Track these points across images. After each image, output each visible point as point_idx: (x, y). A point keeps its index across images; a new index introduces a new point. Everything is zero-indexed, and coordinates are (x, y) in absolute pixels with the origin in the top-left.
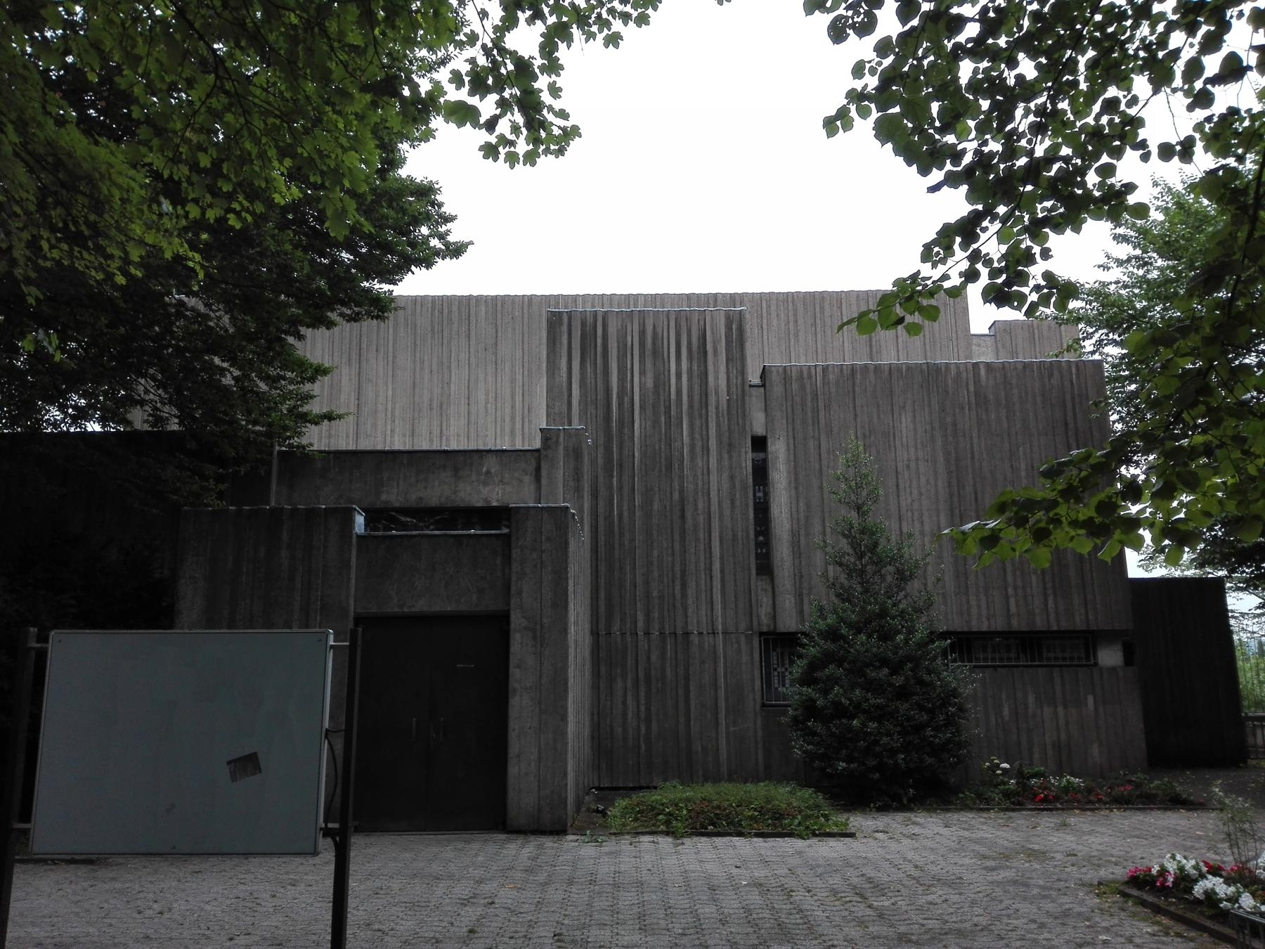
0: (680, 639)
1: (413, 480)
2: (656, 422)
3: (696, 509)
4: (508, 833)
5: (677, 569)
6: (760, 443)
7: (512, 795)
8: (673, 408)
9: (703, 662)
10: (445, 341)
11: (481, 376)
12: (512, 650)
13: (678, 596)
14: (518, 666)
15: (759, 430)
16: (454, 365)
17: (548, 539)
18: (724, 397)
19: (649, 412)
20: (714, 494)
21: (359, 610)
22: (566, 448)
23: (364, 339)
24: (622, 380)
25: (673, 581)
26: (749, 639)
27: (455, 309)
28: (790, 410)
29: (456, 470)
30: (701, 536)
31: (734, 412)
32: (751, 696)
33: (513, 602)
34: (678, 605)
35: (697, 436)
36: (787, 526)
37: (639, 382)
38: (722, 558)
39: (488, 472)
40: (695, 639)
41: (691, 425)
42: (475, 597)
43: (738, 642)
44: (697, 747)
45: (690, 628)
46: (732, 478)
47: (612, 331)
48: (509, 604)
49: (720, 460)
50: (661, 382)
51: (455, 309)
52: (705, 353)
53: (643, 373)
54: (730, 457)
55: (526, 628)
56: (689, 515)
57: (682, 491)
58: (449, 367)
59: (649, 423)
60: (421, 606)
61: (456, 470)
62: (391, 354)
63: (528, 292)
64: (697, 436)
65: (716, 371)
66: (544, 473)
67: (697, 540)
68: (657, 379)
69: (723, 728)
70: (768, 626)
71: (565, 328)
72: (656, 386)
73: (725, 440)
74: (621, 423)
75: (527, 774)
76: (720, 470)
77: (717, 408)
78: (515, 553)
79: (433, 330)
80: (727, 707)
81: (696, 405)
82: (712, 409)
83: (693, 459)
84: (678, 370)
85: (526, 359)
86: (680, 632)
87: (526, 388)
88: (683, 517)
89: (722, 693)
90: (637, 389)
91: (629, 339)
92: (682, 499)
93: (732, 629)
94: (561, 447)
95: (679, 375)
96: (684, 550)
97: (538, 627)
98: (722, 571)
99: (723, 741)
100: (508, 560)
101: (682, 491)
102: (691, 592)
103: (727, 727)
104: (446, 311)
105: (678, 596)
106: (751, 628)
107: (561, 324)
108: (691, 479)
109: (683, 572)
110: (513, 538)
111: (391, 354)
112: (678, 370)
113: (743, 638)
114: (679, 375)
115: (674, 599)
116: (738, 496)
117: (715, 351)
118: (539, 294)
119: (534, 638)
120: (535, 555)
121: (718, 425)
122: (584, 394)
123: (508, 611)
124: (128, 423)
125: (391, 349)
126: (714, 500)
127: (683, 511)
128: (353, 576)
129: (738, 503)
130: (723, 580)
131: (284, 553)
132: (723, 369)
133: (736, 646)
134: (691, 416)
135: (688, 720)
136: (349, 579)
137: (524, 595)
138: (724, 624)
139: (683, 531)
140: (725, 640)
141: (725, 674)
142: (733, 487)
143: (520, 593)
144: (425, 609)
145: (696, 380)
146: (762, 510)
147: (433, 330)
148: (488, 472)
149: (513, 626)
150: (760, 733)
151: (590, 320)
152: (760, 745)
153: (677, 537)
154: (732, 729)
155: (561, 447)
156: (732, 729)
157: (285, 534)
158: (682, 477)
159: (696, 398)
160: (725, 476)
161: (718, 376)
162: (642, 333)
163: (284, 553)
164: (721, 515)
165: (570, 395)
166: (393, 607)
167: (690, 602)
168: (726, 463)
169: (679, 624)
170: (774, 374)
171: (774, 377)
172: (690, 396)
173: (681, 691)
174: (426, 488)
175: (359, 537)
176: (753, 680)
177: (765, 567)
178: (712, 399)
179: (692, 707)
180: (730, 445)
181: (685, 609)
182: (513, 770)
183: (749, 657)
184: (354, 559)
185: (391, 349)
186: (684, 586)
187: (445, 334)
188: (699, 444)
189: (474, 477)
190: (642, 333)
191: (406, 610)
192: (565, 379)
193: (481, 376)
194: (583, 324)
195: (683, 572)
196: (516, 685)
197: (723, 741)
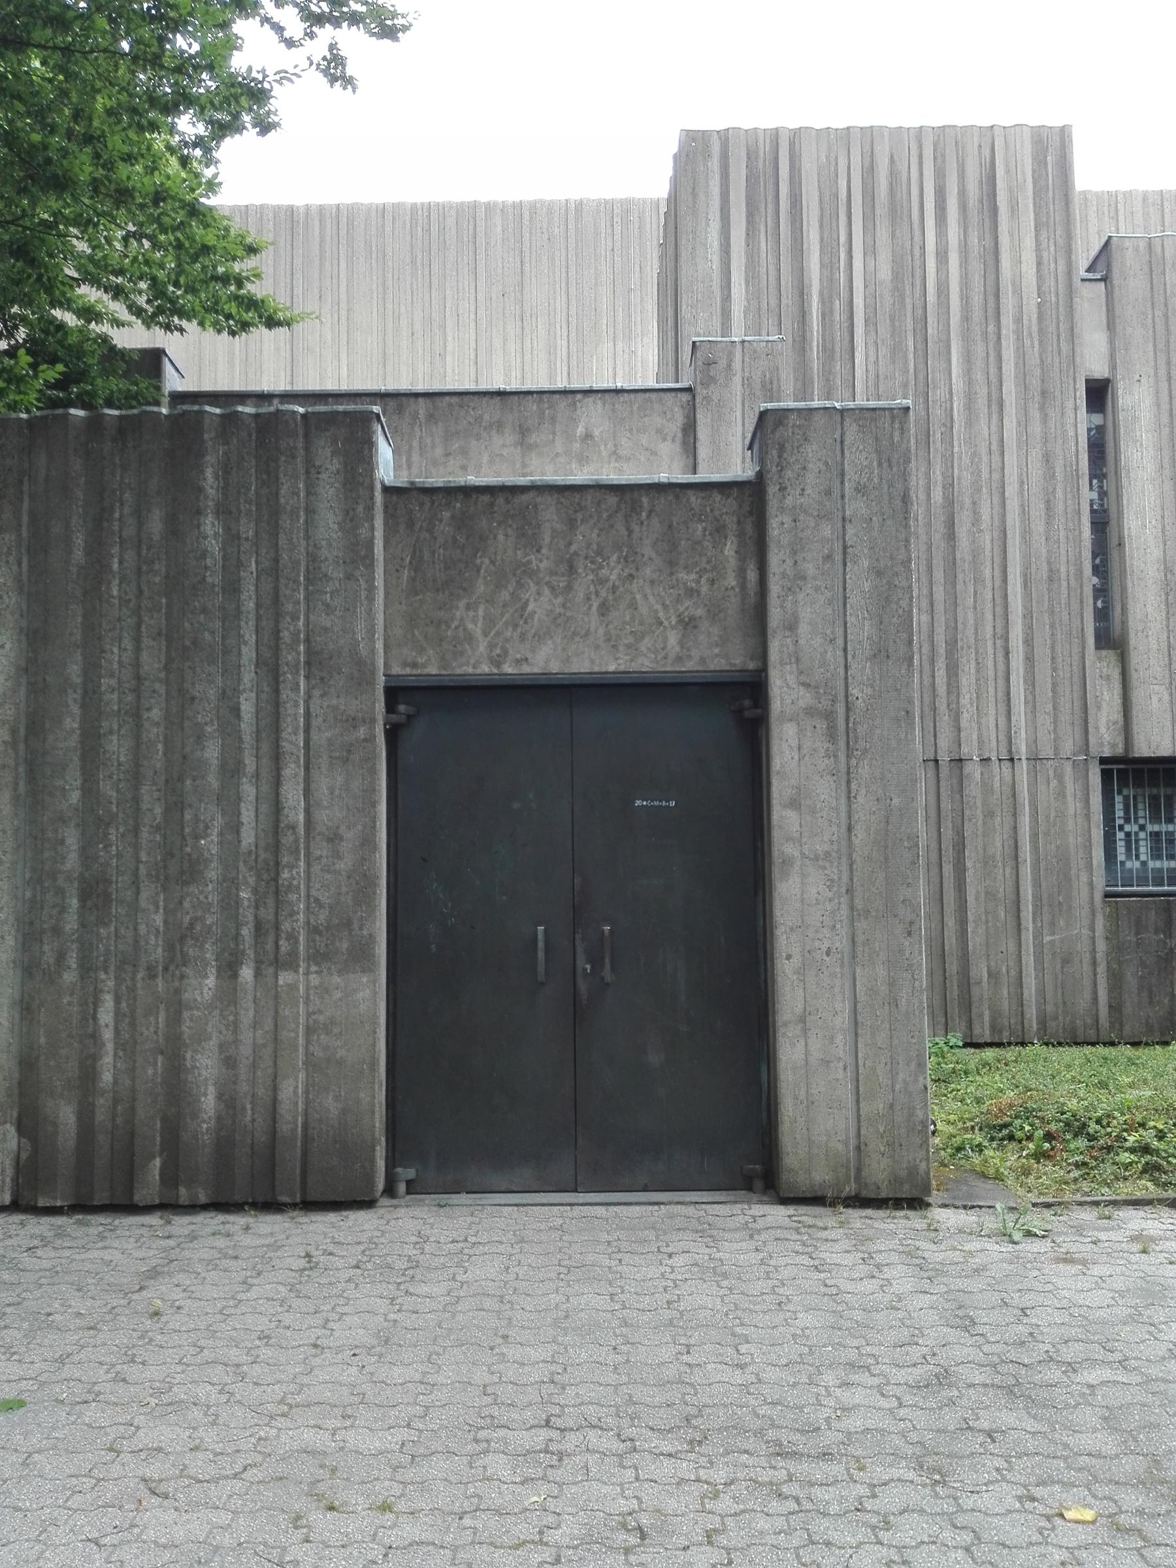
0: (944, 770)
1: (439, 451)
2: (897, 350)
3: (976, 519)
4: (785, 1201)
5: (940, 638)
6: (1098, 394)
7: (789, 1110)
8: (931, 319)
9: (989, 814)
10: (435, 280)
11: (497, 343)
12: (777, 763)
13: (942, 689)
14: (794, 804)
15: (1100, 371)
16: (450, 323)
17: (860, 489)
18: (1032, 301)
19: (884, 330)
20: (1011, 490)
21: (396, 670)
22: (747, 382)
23: (298, 276)
24: (829, 266)
25: (932, 661)
26: (1081, 770)
27: (450, 222)
28: (1160, 327)
29: (523, 431)
30: (987, 572)
31: (1052, 328)
32: (1084, 878)
33: (774, 647)
34: (942, 706)
35: (979, 376)
36: (1156, 553)
37: (867, 271)
38: (1028, 615)
39: (588, 436)
40: (973, 770)
41: (968, 358)
42: (673, 639)
43: (1060, 778)
44: (980, 971)
45: (965, 750)
46: (1047, 458)
47: (809, 167)
48: (764, 656)
49: (1024, 422)
50: (906, 270)
51: (450, 222)
52: (994, 211)
53: (871, 250)
54: (1045, 419)
55: (810, 711)
56: (962, 532)
57: (949, 485)
58: (443, 327)
59: (884, 351)
60: (545, 659)
61: (523, 431)
62: (343, 305)
63: (575, 193)
64: (979, 376)
65: (1017, 249)
66: (703, 433)
67: (978, 580)
68: (898, 263)
69: (1028, 936)
70: (1114, 746)
71: (715, 164)
72: (897, 277)
73: (1035, 382)
74: (828, 352)
75: (826, 1063)
76: (1024, 443)
77: (1019, 320)
78: (778, 525)
79: (413, 262)
80: (1037, 898)
81: (977, 315)
82: (1007, 322)
83: (969, 424)
84: (945, 246)
85: (573, 312)
86: (944, 758)
87: (574, 362)
88: (951, 536)
89: (1027, 871)
90: (858, 283)
91: (843, 184)
92: (950, 502)
93: (1047, 751)
94: (737, 380)
95: (942, 256)
96: (953, 602)
97: (840, 709)
98: (1028, 642)
99: (1029, 961)
100: (758, 547)
101: (949, 485)
102: (967, 680)
103: (1038, 934)
104: (434, 229)
105: (942, 689)
106: (1086, 751)
107: (707, 155)
108: (966, 460)
109: (952, 643)
110: (772, 490)
111: (343, 305)
112: (945, 246)
113: (1068, 768)
114: (942, 256)
115: (934, 695)
116: (1059, 494)
117: (1014, 209)
118: (594, 196)
119: (832, 736)
120: (827, 531)
121: (1021, 354)
122: (754, 295)
123: (763, 670)
124: (73, 731)
125: (343, 297)
126: (1013, 505)
127: (951, 524)
128: (379, 582)
129: (1060, 507)
130: (1029, 659)
131: (210, 525)
132: (1029, 242)
133: (1054, 783)
134: (966, 336)
135: (963, 922)
136: (371, 589)
137: (803, 629)
138: (1034, 742)
139: (952, 565)
140: (1033, 774)
141: (1035, 836)
142: (1050, 475)
143: (791, 626)
144: (555, 667)
145: (976, 267)
146: (1103, 524)
147: (413, 262)
148: (588, 436)
149: (776, 706)
150: (1101, 946)
151: (764, 148)
152: (1102, 969)
153: (939, 575)
154: (1047, 939)
155: (737, 380)
156: (1047, 939)
157: (209, 473)
158: (949, 461)
159: (977, 300)
160: (1036, 454)
161: (1021, 260)
162: (870, 171)
163: (210, 525)
164: (1026, 533)
165: (727, 298)
166: (476, 664)
167: (965, 700)
168: (1036, 428)
169: (944, 743)
170: (1129, 254)
171: (1128, 263)
172: (966, 299)
173: (948, 869)
174: (464, 468)
175: (387, 490)
176: (1088, 847)
177: (1111, 638)
178: (1008, 303)
179: (971, 899)
180: (1043, 393)
181: (957, 717)
182: (791, 1052)
183: (1080, 805)
184: (379, 534)
185: (343, 297)
186: (953, 670)
187: (435, 268)
188: (982, 392)
189: (559, 446)
190: (870, 171)
191: (508, 669)
192: (716, 265)
193: (497, 343)
194: (751, 156)
195: (952, 643)
196: (790, 850)
197: (1029, 961)
